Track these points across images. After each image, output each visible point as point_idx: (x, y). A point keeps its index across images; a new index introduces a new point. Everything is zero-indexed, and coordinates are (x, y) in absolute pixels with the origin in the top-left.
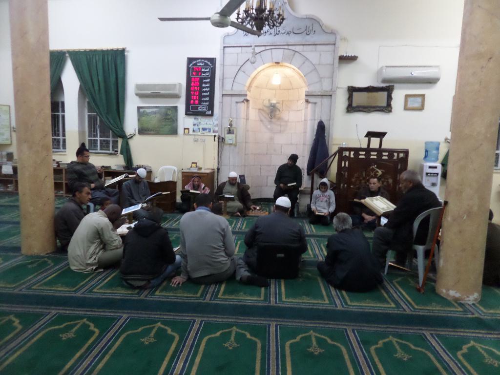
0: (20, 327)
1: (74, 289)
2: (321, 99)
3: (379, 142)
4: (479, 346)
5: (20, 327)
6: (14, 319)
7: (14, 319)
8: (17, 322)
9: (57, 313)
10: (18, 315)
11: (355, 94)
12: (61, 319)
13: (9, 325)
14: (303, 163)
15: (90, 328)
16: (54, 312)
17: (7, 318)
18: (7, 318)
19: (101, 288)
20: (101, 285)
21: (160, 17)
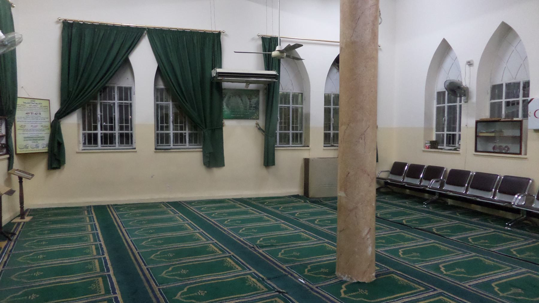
0: (400, 251)
1: (441, 297)
2: (18, 98)
3: (517, 152)
4: (458, 216)
5: (400, 251)
6: (444, 271)
7: (444, 271)
8: (442, 269)
9: (464, 283)
10: (399, 256)
11: (519, 152)
12: (462, 279)
13: (404, 253)
14: (232, 97)
15: (498, 288)
16: (467, 285)
17: (405, 256)
18: (405, 256)
19: (416, 289)
20: (415, 291)
21: (533, 100)
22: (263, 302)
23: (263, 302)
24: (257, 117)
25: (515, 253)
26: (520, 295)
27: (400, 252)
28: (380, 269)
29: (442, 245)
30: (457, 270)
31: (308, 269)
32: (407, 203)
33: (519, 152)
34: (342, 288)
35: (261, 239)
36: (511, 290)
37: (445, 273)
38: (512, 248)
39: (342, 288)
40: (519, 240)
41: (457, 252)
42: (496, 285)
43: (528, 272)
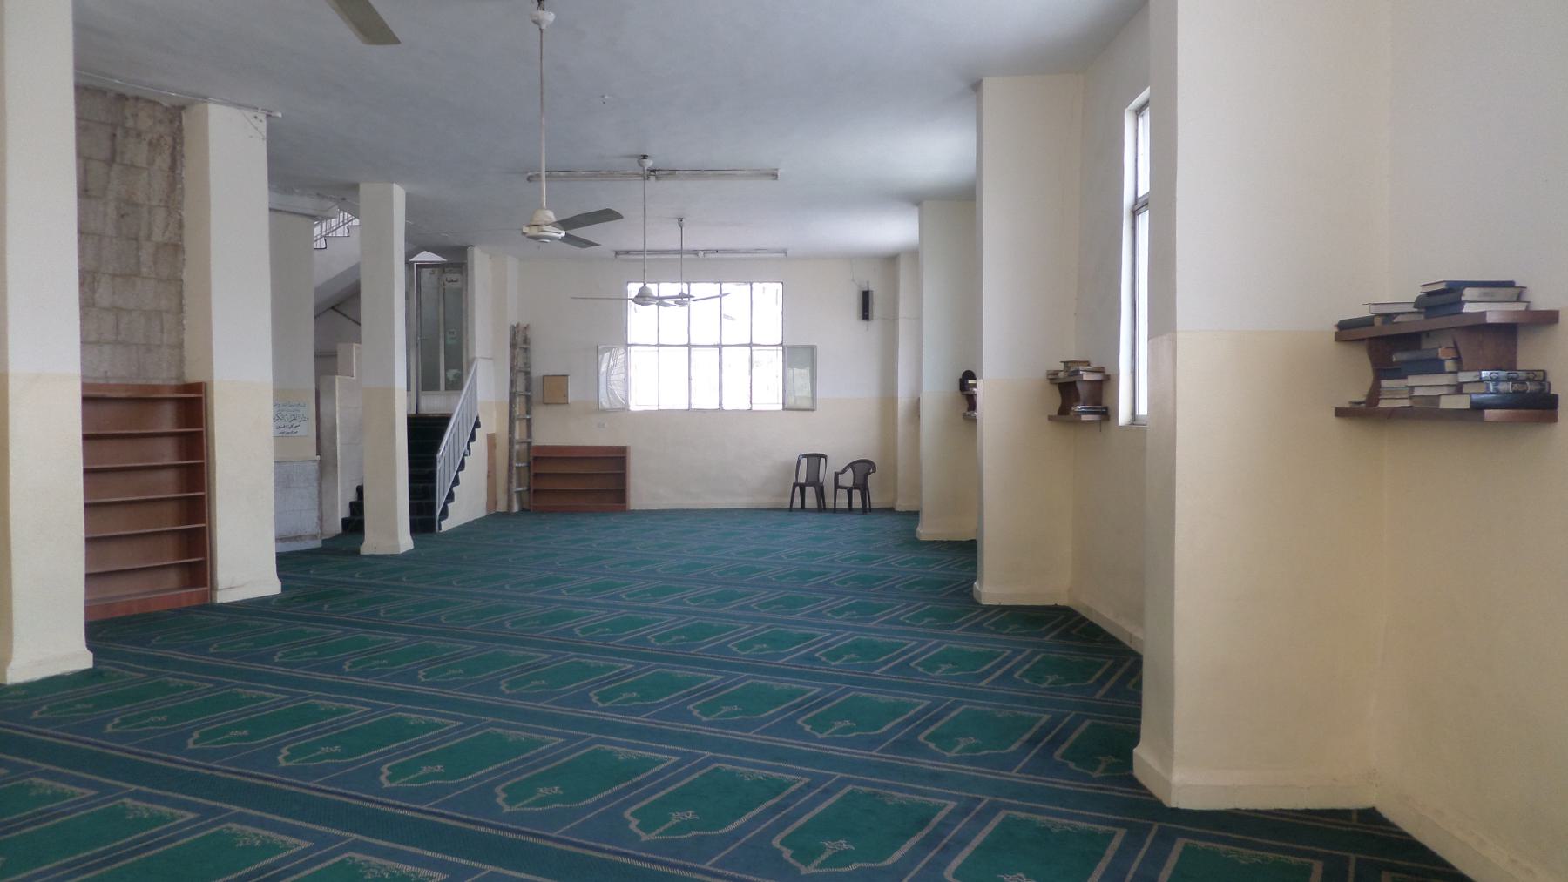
22: (257, 879)
23: (257, 879)
24: (166, 420)
25: (735, 649)
26: (850, 730)
27: (592, 698)
28: (372, 711)
29: (591, 658)
30: (725, 709)
31: (283, 756)
32: (507, 587)
33: (855, 466)
34: (382, 773)
35: (196, 735)
36: (722, 709)
37: (508, 692)
38: (730, 642)
39: (382, 773)
40: (593, 613)
41: (713, 678)
42: (804, 722)
43: (749, 677)
